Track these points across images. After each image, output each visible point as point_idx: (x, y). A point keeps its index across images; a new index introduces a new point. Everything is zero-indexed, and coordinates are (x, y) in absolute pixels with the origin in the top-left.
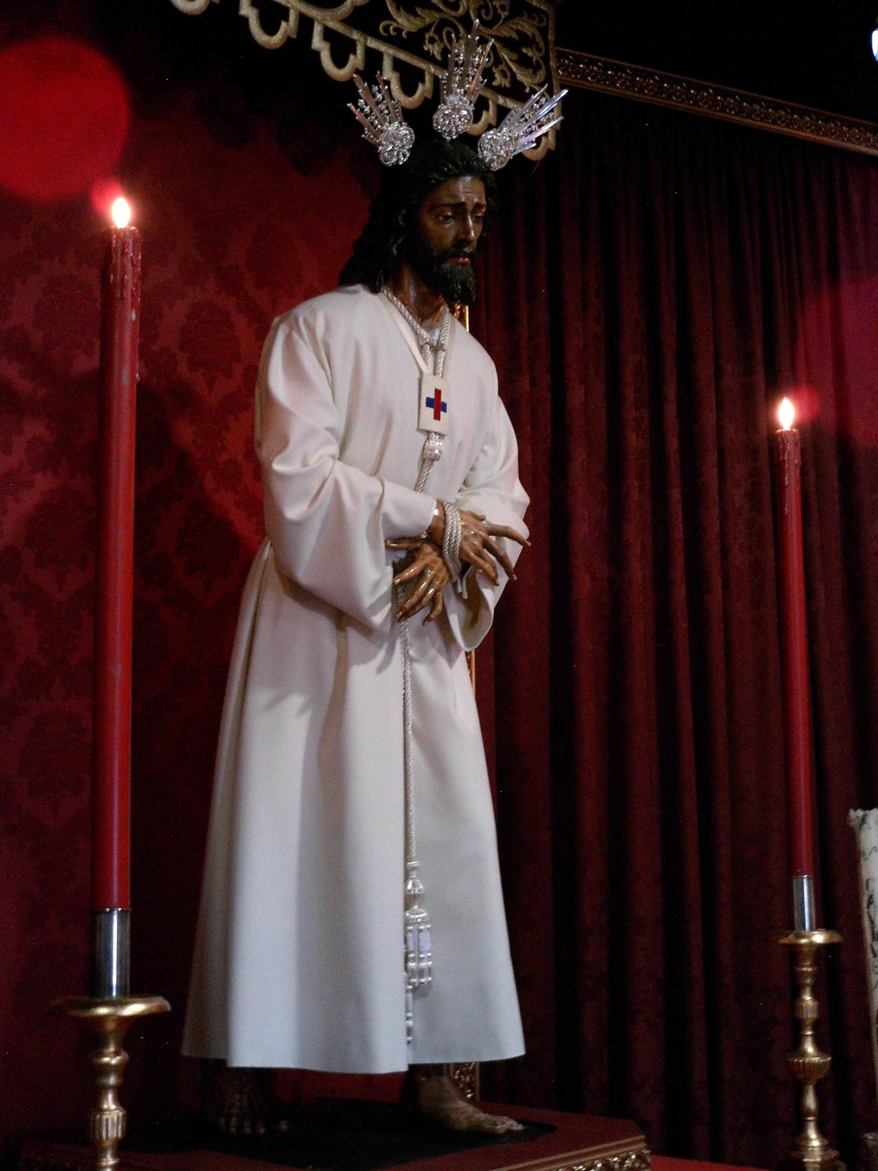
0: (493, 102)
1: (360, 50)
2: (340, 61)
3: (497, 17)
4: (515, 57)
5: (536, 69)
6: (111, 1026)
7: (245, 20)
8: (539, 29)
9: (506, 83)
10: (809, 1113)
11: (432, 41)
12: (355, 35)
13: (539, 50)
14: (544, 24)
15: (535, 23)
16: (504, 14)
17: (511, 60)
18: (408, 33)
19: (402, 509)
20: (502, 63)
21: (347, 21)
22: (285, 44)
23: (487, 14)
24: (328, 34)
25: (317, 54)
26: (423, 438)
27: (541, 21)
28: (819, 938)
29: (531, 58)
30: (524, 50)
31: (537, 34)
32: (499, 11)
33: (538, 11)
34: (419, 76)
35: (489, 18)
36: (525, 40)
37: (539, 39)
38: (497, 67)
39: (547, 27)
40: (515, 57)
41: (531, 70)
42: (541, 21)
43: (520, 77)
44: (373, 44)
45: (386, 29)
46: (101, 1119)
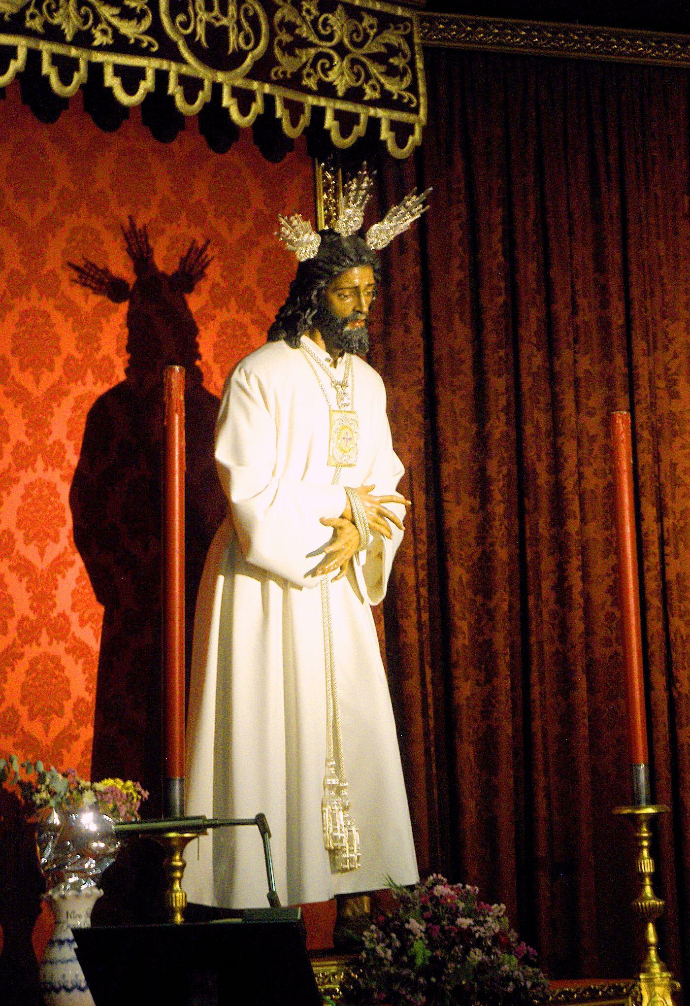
0: (280, 97)
1: (82, 65)
2: (66, 79)
3: (367, 37)
4: (383, 69)
5: (139, 17)
6: (643, 818)
7: (110, 89)
8: (403, 36)
9: (376, 95)
10: (642, 876)
11: (309, 75)
12: (255, 85)
13: (405, 56)
14: (408, 31)
15: (400, 32)
16: (372, 33)
17: (381, 73)
18: (11, 16)
19: (78, 580)
20: (101, 22)
21: (251, 75)
22: (146, 98)
23: (358, 37)
24: (236, 92)
25: (47, 78)
26: (355, 410)
27: (406, 28)
28: (650, 810)
29: (397, 67)
30: (391, 60)
31: (401, 41)
32: (368, 31)
33: (402, 19)
34: (140, 73)
35: (359, 40)
36: (393, 51)
37: (405, 47)
38: (95, 28)
39: (412, 33)
40: (383, 69)
41: (398, 78)
42: (406, 28)
43: (388, 87)
44: (267, 88)
45: (276, 74)
46: (397, 895)
